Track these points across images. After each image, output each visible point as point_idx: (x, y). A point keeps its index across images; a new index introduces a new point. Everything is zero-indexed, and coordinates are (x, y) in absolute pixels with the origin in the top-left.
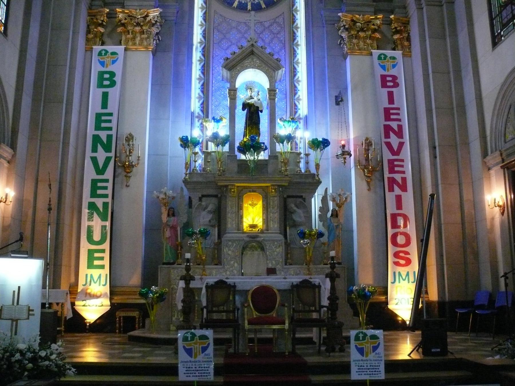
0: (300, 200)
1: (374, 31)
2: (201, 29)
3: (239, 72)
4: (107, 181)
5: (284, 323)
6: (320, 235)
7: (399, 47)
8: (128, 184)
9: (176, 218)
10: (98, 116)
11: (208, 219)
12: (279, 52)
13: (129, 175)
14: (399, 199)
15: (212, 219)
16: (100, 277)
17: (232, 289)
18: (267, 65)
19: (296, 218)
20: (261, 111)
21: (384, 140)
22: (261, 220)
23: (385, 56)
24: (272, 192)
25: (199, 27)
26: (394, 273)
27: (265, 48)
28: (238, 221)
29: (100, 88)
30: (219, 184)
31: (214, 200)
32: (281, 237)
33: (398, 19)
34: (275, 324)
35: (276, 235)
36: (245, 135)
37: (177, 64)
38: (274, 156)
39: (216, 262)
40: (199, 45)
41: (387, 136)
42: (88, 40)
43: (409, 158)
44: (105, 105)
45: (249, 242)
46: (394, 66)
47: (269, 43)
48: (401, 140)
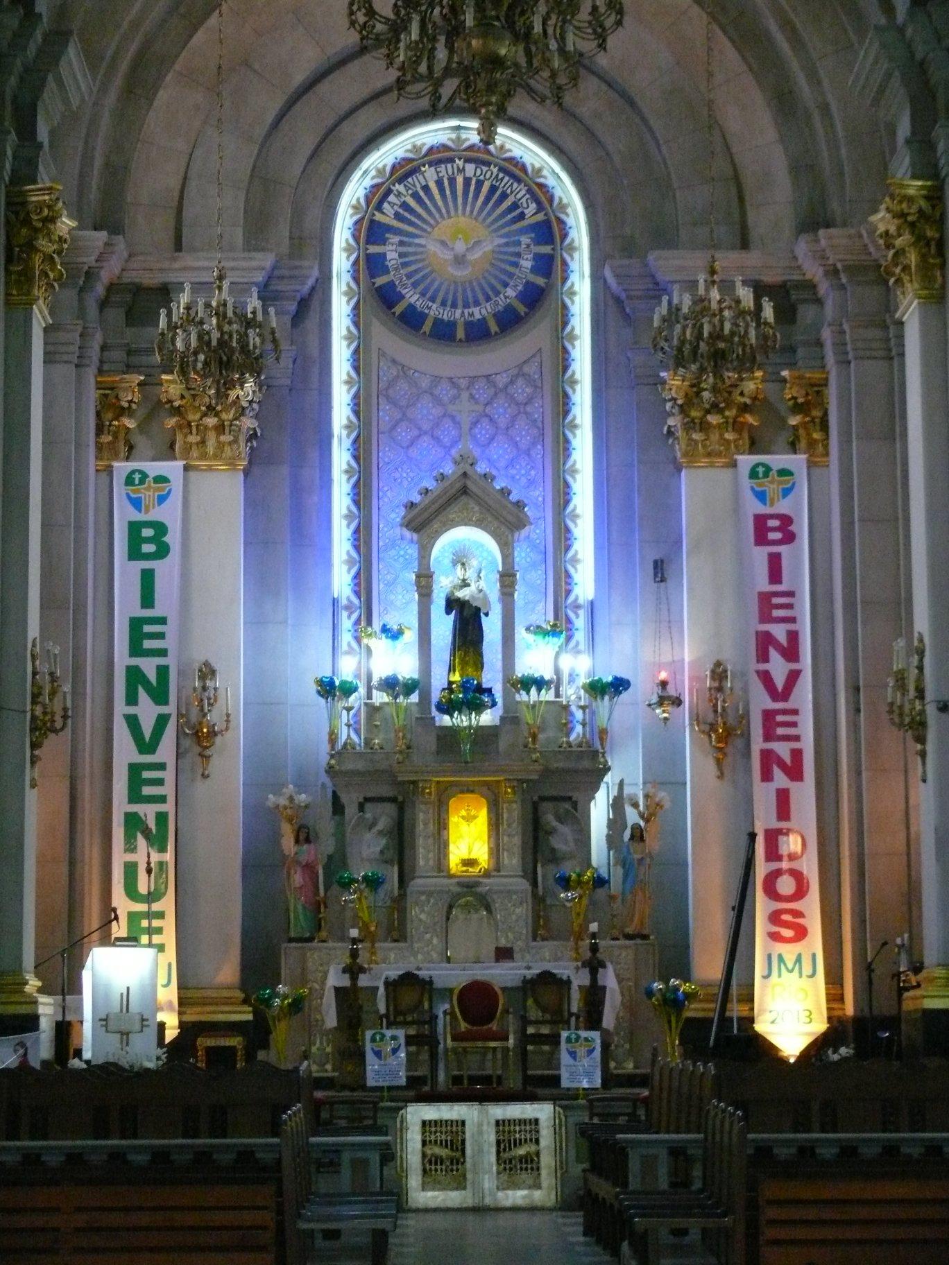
0: (567, 806)
1: (745, 408)
2: (349, 391)
3: (438, 534)
4: (161, 767)
5: (507, 1039)
6: (600, 882)
7: (803, 444)
8: (207, 772)
9: (312, 846)
10: (136, 625)
11: (378, 849)
12: (529, 449)
13: (208, 752)
14: (783, 798)
15: (387, 847)
16: (799, 960)
17: (427, 987)
18: (497, 518)
19: (556, 842)
20: (487, 614)
21: (754, 666)
22: (485, 849)
23: (768, 469)
24: (506, 792)
25: (345, 388)
26: (769, 957)
27: (493, 478)
28: (439, 849)
29: (134, 559)
30: (400, 779)
31: (390, 809)
32: (525, 885)
33: (801, 377)
34: (495, 1040)
35: (515, 880)
36: (451, 669)
37: (298, 490)
38: (511, 718)
39: (395, 935)
40: (345, 433)
41: (763, 657)
42: (99, 447)
43: (810, 706)
44: (147, 599)
45: (459, 896)
46: (786, 492)
47: (507, 429)
48: (794, 666)
